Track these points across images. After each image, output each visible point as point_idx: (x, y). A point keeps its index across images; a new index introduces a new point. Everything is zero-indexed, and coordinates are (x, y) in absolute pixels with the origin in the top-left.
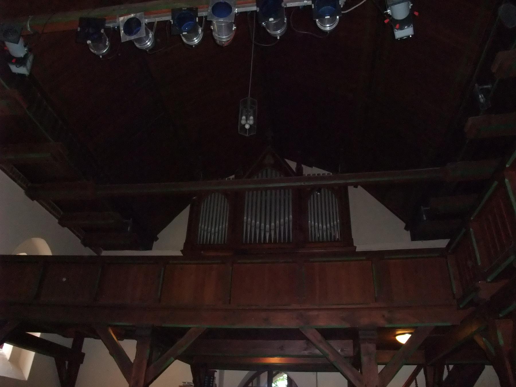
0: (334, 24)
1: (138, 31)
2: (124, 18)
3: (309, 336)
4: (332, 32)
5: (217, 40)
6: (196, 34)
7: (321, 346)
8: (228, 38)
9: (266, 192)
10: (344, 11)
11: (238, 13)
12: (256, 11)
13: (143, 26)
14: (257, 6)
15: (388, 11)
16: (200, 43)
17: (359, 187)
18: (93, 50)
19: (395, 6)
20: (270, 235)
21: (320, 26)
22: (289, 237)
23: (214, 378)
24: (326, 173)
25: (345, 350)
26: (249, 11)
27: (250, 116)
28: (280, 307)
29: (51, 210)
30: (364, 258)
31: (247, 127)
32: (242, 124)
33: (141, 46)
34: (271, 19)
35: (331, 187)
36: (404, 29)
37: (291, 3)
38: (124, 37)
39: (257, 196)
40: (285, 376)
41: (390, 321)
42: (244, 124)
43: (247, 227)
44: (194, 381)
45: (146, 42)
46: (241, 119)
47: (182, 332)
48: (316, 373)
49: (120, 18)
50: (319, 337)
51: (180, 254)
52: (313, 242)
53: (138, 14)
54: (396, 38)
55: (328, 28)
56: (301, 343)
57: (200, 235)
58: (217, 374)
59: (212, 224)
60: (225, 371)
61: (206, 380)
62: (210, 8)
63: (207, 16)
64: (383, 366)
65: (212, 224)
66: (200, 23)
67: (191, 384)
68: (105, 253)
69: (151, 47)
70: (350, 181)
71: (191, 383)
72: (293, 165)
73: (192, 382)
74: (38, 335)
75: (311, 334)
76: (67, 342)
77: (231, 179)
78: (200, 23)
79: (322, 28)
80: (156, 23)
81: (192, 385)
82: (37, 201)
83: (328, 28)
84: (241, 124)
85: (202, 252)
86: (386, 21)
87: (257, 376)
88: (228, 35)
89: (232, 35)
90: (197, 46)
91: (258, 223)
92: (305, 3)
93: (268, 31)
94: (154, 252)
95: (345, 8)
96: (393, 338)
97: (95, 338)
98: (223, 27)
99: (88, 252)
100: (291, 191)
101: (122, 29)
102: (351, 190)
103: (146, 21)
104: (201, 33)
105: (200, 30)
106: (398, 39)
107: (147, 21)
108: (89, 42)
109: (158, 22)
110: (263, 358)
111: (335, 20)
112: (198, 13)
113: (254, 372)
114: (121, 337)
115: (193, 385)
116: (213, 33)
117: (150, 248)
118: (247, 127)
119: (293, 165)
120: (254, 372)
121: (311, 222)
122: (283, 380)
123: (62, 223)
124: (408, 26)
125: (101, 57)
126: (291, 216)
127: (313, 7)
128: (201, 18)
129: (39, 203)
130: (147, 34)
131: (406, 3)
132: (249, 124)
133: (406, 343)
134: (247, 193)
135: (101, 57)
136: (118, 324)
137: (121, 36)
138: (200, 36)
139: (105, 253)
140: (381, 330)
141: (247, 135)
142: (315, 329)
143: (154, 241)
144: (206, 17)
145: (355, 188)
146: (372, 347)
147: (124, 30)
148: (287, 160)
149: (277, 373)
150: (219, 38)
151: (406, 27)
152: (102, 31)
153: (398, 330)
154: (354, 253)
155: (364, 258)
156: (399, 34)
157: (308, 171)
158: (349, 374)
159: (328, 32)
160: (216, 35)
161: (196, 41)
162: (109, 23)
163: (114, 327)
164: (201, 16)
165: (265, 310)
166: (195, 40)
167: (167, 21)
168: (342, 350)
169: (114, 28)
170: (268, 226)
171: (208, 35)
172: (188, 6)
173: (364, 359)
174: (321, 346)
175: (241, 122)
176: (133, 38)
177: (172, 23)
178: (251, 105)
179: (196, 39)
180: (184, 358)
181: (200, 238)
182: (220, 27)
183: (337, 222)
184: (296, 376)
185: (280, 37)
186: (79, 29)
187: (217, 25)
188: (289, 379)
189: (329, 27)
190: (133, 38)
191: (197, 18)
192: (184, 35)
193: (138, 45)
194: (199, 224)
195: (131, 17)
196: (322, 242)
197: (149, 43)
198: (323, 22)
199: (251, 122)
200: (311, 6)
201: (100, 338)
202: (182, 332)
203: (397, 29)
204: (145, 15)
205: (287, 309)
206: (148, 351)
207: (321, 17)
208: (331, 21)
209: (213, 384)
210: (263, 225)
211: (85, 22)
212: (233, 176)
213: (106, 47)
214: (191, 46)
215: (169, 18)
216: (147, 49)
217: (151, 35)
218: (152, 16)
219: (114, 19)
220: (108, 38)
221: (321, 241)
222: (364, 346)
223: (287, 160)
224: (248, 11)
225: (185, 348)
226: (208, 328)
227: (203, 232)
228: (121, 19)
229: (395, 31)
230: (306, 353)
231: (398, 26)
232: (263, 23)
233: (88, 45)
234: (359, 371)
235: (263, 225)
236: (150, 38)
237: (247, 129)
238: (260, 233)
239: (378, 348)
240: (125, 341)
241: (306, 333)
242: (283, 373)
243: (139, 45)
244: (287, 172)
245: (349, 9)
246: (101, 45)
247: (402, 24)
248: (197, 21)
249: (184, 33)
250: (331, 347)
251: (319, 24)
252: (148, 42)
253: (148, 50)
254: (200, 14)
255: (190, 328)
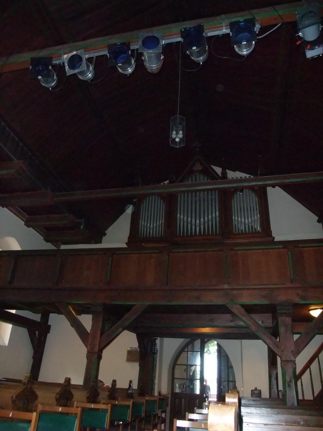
0: (250, 49)
1: (81, 65)
2: (68, 55)
3: (234, 310)
4: (249, 55)
5: (148, 69)
6: (130, 64)
7: (244, 319)
8: (157, 66)
9: (196, 194)
10: (259, 36)
11: (165, 44)
12: (180, 42)
13: (84, 60)
14: (182, 38)
15: (300, 34)
16: (133, 73)
17: (277, 187)
18: (43, 83)
19: (306, 29)
20: (200, 229)
21: (239, 51)
22: (216, 230)
23: (155, 344)
24: (248, 176)
25: (265, 322)
26: (175, 42)
27: (179, 131)
28: (210, 288)
29: (17, 213)
30: (281, 247)
31: (177, 140)
32: (173, 138)
33: (83, 77)
34: (194, 48)
35: (252, 188)
36: (314, 49)
37: (211, 33)
38: (69, 71)
39: (188, 197)
40: (216, 342)
41: (303, 298)
42: (174, 137)
43: (180, 223)
44: (139, 346)
45: (87, 74)
46: (172, 133)
47: (128, 308)
48: (240, 340)
49: (64, 56)
50: (243, 310)
51: (125, 246)
52: (237, 234)
53: (79, 51)
54: (307, 58)
55: (245, 52)
56: (228, 316)
57: (141, 231)
58: (158, 341)
59: (184, 212)
60: (165, 338)
61: (149, 345)
62: (140, 42)
63: (138, 49)
64: (298, 336)
65: (184, 212)
66: (132, 55)
67: (137, 349)
68: (63, 247)
69: (92, 78)
70: (268, 182)
71: (137, 348)
72: (218, 170)
73: (138, 347)
74: (14, 311)
75: (236, 309)
76: (37, 317)
77: (166, 184)
78: (132, 55)
79: (240, 53)
80: (95, 58)
81: (138, 350)
82: (6, 207)
83: (245, 52)
84: (172, 138)
85: (143, 244)
86: (298, 43)
87: (191, 342)
88: (157, 64)
89: (160, 64)
90: (131, 75)
91: (189, 219)
92: (224, 32)
93: (192, 58)
94: (105, 244)
95: (258, 35)
96: (307, 312)
97: (59, 314)
98: (153, 57)
99: (49, 246)
100: (217, 192)
101: (67, 65)
102: (269, 190)
103: (87, 56)
104: (134, 64)
105: (133, 61)
106: (309, 58)
107: (87, 56)
108: (40, 77)
109: (96, 56)
110: (197, 328)
111: (251, 45)
112: (131, 47)
113: (188, 340)
114: (80, 313)
115: (138, 349)
116: (145, 63)
117: (100, 242)
118: (177, 140)
119: (218, 170)
120: (188, 340)
121: (235, 218)
122: (214, 346)
123: (28, 224)
124: (319, 46)
125: (50, 89)
126: (217, 213)
127: (231, 35)
128: (133, 51)
129: (9, 209)
130: (88, 67)
131: (316, 26)
132: (179, 138)
133: (318, 317)
134: (179, 194)
135: (50, 89)
136: (76, 302)
137: (66, 70)
138: (133, 66)
139: (63, 247)
140: (296, 305)
141: (178, 147)
142: (240, 305)
143: (103, 236)
144: (137, 50)
145: (106, 236)
146: (288, 320)
147: (68, 65)
148: (213, 166)
149: (209, 340)
150: (150, 66)
151: (316, 47)
152: (50, 68)
153: (311, 306)
154: (273, 242)
155: (281, 247)
156: (310, 54)
157: (231, 175)
158: (268, 341)
159: (246, 56)
160: (147, 64)
161: (130, 70)
162: (56, 60)
163: (73, 306)
164: (132, 49)
165: (196, 290)
166: (129, 70)
167: (105, 55)
168: (263, 322)
169: (60, 64)
170: (198, 221)
171: (140, 65)
172: (122, 42)
173: (282, 330)
174: (244, 319)
175: (171, 136)
176: (76, 71)
177: (109, 57)
178: (180, 122)
179: (130, 69)
180: (131, 328)
181: (141, 233)
182: (149, 57)
183: (257, 217)
184: (226, 343)
185: (203, 63)
186: (31, 67)
187: (147, 56)
188: (218, 345)
189: (246, 51)
190: (76, 71)
191: (130, 51)
192: (120, 67)
193: (80, 77)
194: (139, 222)
195: (74, 54)
196: (249, 233)
197: (90, 75)
198: (240, 47)
199: (181, 136)
200: (229, 34)
201: (62, 314)
202: (128, 308)
203: (308, 50)
204: (85, 51)
205: (216, 289)
206: (101, 323)
207: (239, 43)
208: (249, 45)
209: (154, 349)
210: (193, 220)
211: (35, 62)
212: (168, 181)
213: (54, 80)
214: (126, 75)
215: (105, 52)
216: (88, 80)
217: (91, 68)
218: (91, 52)
219: (60, 56)
220: (56, 72)
221: (244, 233)
222: (280, 319)
223: (213, 166)
224: (174, 42)
225: (131, 321)
226: (149, 305)
227: (143, 227)
228: (65, 56)
229: (306, 51)
230: (232, 324)
231: (309, 47)
232: (187, 52)
233: (39, 80)
234: (278, 340)
235: (193, 220)
236: (91, 71)
237: (177, 142)
238: (191, 228)
239: (294, 320)
240: (83, 316)
241: (232, 308)
242: (213, 340)
243: (82, 77)
244: (213, 176)
245: (265, 34)
246: (50, 79)
247: (313, 44)
248: (130, 53)
249: (119, 65)
250: (253, 319)
251: (237, 50)
252: (89, 74)
253: (89, 81)
254: (132, 47)
255: (134, 305)
